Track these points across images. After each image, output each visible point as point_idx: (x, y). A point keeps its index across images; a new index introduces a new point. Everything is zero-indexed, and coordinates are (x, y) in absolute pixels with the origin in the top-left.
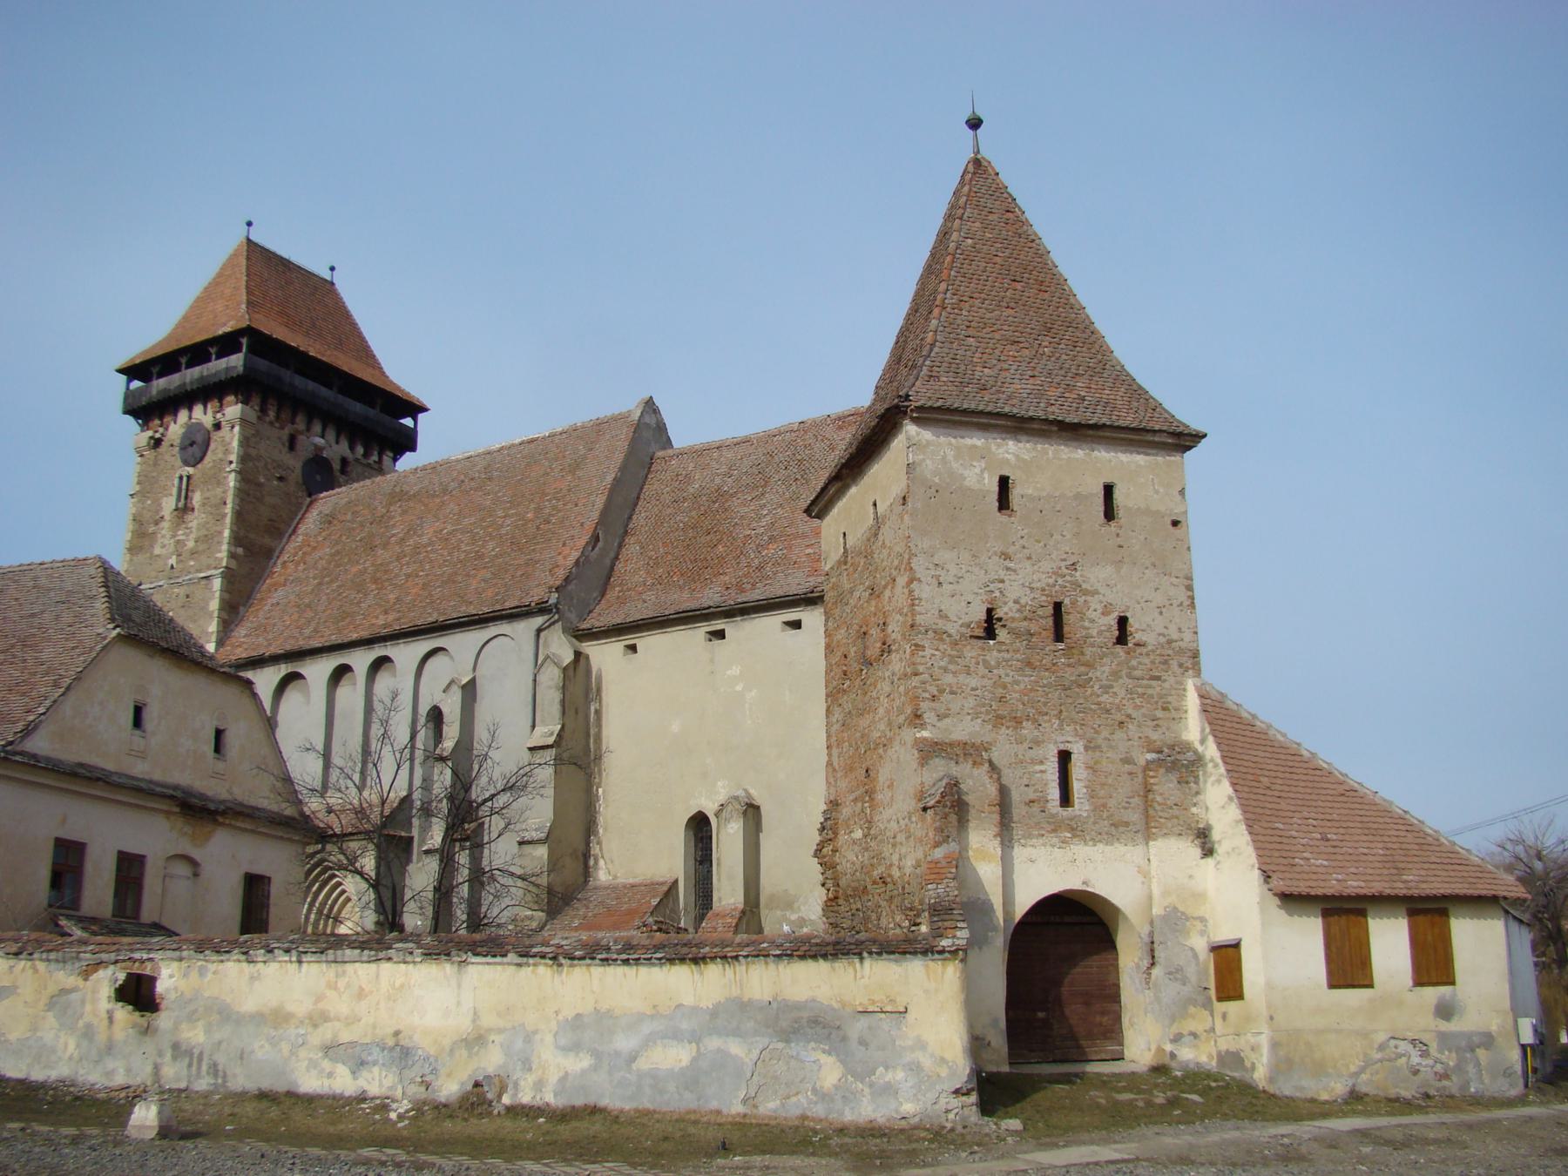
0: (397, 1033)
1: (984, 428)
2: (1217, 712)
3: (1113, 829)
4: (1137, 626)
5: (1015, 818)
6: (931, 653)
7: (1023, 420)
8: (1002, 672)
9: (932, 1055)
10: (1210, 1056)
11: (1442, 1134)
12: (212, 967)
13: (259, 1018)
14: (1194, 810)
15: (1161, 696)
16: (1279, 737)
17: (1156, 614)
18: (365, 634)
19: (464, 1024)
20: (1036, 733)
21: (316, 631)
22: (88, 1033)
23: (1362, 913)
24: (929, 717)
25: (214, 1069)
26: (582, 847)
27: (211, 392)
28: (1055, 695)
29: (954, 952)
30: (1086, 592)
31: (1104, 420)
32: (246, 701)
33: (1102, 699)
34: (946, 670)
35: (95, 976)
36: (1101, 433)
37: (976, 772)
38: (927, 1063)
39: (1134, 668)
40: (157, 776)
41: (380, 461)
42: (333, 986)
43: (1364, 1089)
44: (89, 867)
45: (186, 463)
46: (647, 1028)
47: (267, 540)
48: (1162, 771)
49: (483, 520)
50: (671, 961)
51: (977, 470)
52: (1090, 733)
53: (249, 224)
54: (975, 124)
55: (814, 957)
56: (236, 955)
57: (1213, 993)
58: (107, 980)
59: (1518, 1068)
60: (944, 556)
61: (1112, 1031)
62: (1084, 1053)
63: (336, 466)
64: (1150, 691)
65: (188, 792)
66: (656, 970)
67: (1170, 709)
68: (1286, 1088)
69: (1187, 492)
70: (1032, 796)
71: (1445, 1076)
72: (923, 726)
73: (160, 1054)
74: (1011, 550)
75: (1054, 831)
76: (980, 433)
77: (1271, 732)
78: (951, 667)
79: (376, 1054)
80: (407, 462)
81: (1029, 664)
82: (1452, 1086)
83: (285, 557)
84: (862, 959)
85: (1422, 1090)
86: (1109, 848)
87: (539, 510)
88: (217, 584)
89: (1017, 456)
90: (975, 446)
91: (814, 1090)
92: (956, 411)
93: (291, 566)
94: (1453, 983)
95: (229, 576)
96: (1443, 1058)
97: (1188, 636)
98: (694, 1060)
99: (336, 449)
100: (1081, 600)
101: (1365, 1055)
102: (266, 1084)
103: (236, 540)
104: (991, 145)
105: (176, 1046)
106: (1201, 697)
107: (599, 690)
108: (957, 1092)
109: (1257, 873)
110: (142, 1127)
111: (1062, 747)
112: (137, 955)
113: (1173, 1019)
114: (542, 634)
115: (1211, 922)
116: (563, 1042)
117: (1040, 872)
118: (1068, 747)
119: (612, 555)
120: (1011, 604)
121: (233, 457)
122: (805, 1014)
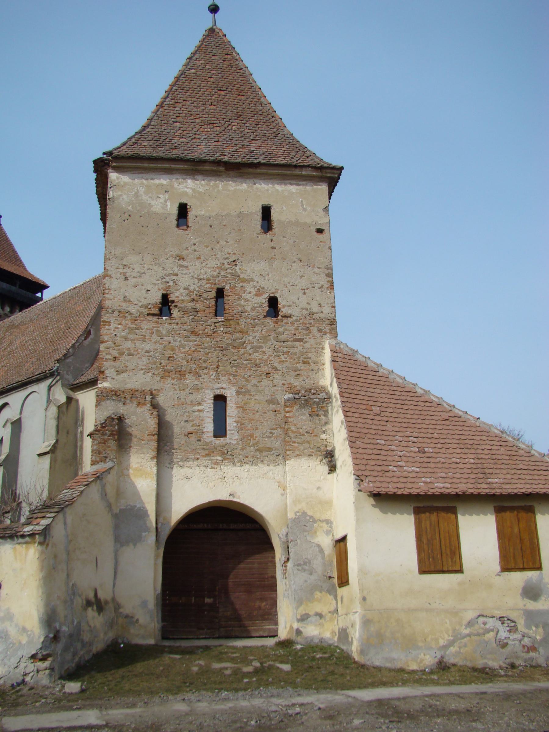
1: (169, 171)
2: (348, 365)
4: (283, 303)
8: (171, 339)
9: (17, 625)
10: (333, 632)
11: (462, 705)
14: (323, 436)
16: (398, 380)
17: (301, 294)
20: (196, 382)
23: (453, 511)
28: (213, 356)
29: (32, 535)
30: (244, 281)
33: (253, 356)
34: (126, 339)
36: (258, 171)
37: (139, 410)
39: (280, 334)
43: (452, 660)
49: (42, 332)
51: (162, 200)
52: (242, 381)
54: (214, 9)
57: (336, 581)
60: (132, 259)
61: (270, 614)
62: (248, 631)
64: (292, 350)
67: (309, 362)
68: (376, 659)
70: (190, 428)
74: (185, 253)
75: (207, 455)
76: (165, 176)
81: (194, 332)
85: (508, 661)
86: (253, 468)
90: (162, 185)
94: (540, 568)
97: (327, 310)
101: (454, 630)
104: (222, 21)
106: (333, 351)
107: (83, 419)
109: (353, 477)
111: (218, 392)
114: (52, 389)
115: (334, 523)
117: (194, 488)
118: (222, 392)
120: (182, 290)
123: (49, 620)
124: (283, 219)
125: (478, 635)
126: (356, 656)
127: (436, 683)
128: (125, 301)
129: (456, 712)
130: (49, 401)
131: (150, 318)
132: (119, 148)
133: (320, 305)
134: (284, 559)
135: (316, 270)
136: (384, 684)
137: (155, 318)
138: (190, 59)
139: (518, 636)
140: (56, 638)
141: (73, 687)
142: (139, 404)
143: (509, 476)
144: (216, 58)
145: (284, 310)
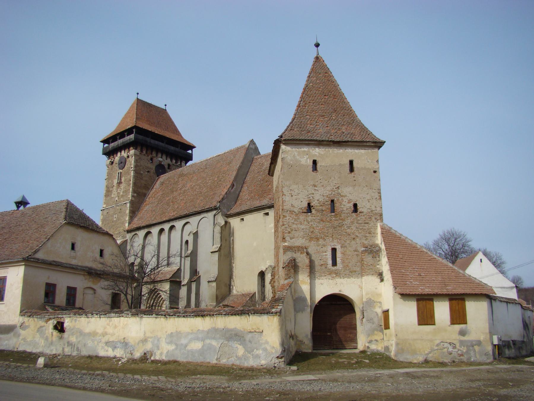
0: (124, 338)
2: (387, 234)
3: (350, 273)
5: (316, 270)
6: (289, 218)
7: (320, 141)
8: (312, 223)
10: (382, 348)
11: (435, 374)
12: (78, 319)
13: (90, 334)
14: (378, 266)
15: (368, 229)
17: (367, 202)
18: (167, 219)
19: (141, 335)
20: (324, 242)
21: (155, 218)
22: (47, 339)
23: (432, 300)
24: (287, 238)
25: (78, 349)
26: (228, 283)
27: (126, 147)
28: (331, 230)
29: (276, 313)
30: (342, 196)
31: (350, 140)
32: (111, 240)
34: (293, 223)
35: (49, 322)
36: (348, 144)
37: (302, 256)
38: (269, 348)
39: (359, 220)
40: (80, 264)
41: (181, 164)
42: (108, 325)
43: (430, 359)
44: (57, 291)
45: (120, 169)
46: (190, 337)
47: (144, 191)
48: (367, 254)
49: (203, 181)
50: (196, 316)
51: (305, 159)
53: (138, 94)
54: (317, 45)
55: (235, 315)
56: (84, 316)
57: (383, 327)
58: (51, 323)
59: (491, 353)
60: (294, 187)
61: (354, 340)
62: (345, 346)
63: (166, 167)
65: (90, 269)
66: (192, 319)
67: (371, 233)
68: (401, 358)
69: (379, 161)
70: (322, 263)
71: (462, 355)
72: (285, 242)
73: (64, 345)
74: (316, 184)
75: (330, 274)
77: (407, 240)
78: (295, 222)
79: (119, 345)
80: (190, 163)
81: (322, 220)
82: (464, 358)
83: (150, 196)
84: (249, 315)
86: (349, 279)
87: (218, 177)
88: (128, 205)
89: (319, 153)
90: (305, 151)
91: (236, 356)
92: (297, 140)
93: (151, 198)
94: (466, 323)
95: (132, 203)
96: (461, 349)
97: (378, 209)
98: (203, 347)
99: (165, 161)
100: (341, 199)
102: (91, 353)
103: (134, 191)
104: (323, 53)
105: (68, 342)
106: (382, 229)
107: (233, 233)
108: (278, 357)
109: (392, 287)
110: (40, 364)
111: (333, 247)
112: (59, 316)
113: (369, 335)
116: (168, 341)
117: (325, 288)
119: (239, 190)
120: (316, 201)
121: (132, 166)
122: (233, 333)
123: (283, 344)
124: (359, 166)
125: (441, 349)
126: (393, 357)
127: (424, 367)
128: (292, 206)
129: (433, 376)
130: (214, 225)
131: (303, 214)
132: (285, 132)
133: (376, 207)
134: (361, 317)
135: (374, 191)
136: (406, 367)
137: (305, 214)
138: (309, 77)
139: (456, 350)
140: (284, 351)
141: (294, 368)
142: (301, 253)
143: (455, 286)
144: (321, 75)
145: (360, 210)
